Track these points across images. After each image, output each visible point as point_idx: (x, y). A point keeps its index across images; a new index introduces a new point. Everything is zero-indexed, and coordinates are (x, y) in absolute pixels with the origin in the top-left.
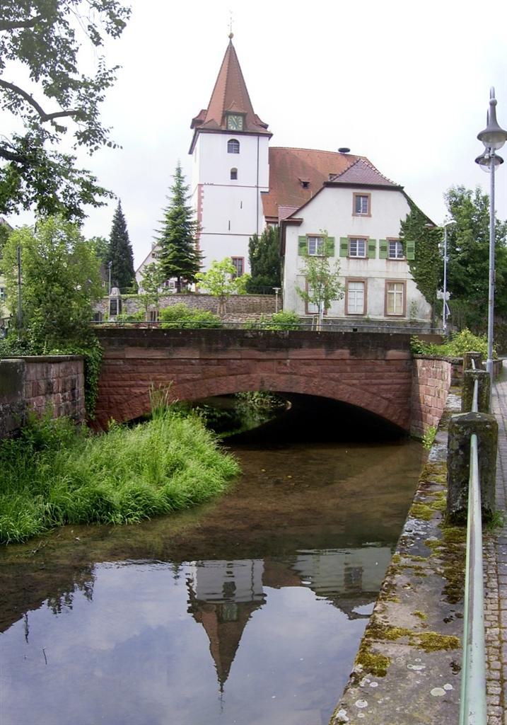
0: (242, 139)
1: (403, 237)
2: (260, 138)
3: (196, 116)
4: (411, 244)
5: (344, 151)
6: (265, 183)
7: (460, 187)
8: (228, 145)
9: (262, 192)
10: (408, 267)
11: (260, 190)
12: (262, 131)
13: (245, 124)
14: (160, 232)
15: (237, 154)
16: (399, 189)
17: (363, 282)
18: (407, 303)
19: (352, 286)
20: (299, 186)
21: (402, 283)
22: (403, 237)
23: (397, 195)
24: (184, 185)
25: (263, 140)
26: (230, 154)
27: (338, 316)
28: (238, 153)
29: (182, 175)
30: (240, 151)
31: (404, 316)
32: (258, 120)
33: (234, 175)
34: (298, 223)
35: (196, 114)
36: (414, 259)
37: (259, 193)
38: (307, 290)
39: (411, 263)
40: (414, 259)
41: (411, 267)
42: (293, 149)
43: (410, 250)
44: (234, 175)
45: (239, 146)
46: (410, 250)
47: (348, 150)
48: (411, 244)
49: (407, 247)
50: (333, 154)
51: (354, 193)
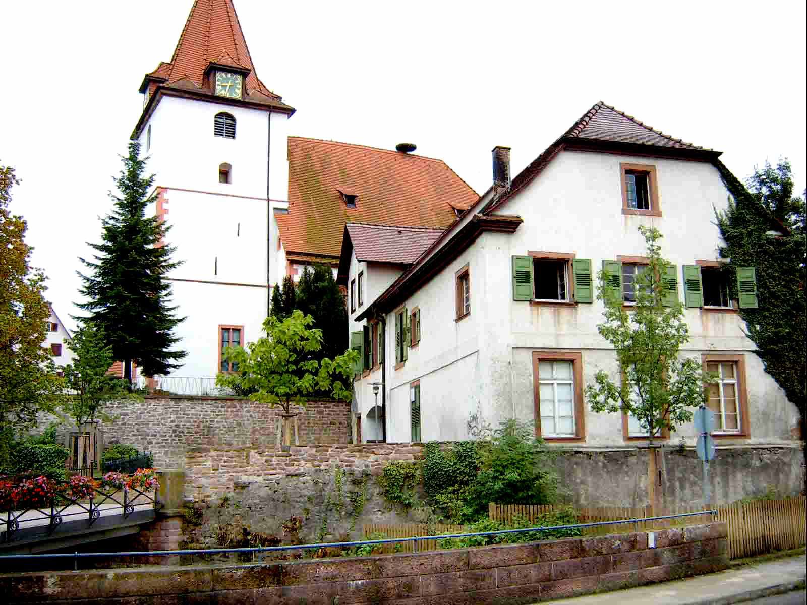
0: (238, 113)
1: (728, 260)
2: (274, 116)
3: (151, 72)
4: (746, 274)
5: (405, 149)
6: (281, 192)
7: (782, 163)
8: (216, 123)
9: (275, 209)
10: (744, 324)
11: (273, 205)
12: (275, 103)
13: (245, 90)
14: (89, 264)
15: (231, 140)
16: (710, 158)
17: (572, 361)
18: (751, 410)
19: (545, 372)
20: (340, 202)
21: (733, 363)
22: (728, 260)
23: (706, 173)
24: (144, 176)
25: (278, 120)
26: (220, 138)
27: (611, 443)
28: (234, 137)
29: (140, 158)
30: (236, 135)
31: (744, 435)
32: (262, 88)
33: (225, 174)
34: (511, 226)
35: (151, 68)
36: (756, 306)
37: (271, 211)
38: (624, 385)
39: (748, 315)
40: (756, 306)
41: (750, 324)
42: (322, 142)
43: (747, 288)
44: (225, 174)
45: (234, 125)
46: (747, 288)
47: (413, 148)
48: (746, 274)
49: (739, 279)
50: (388, 153)
51: (621, 164)
